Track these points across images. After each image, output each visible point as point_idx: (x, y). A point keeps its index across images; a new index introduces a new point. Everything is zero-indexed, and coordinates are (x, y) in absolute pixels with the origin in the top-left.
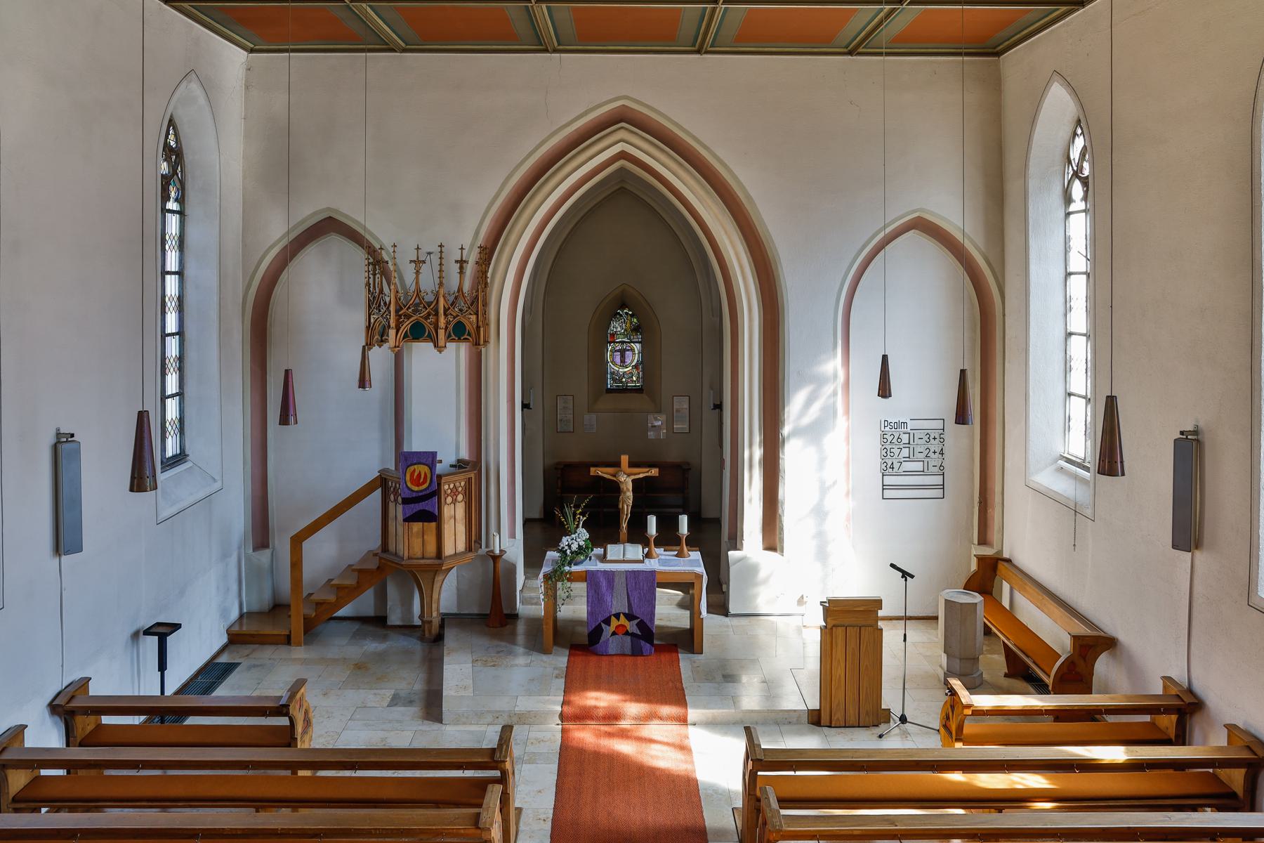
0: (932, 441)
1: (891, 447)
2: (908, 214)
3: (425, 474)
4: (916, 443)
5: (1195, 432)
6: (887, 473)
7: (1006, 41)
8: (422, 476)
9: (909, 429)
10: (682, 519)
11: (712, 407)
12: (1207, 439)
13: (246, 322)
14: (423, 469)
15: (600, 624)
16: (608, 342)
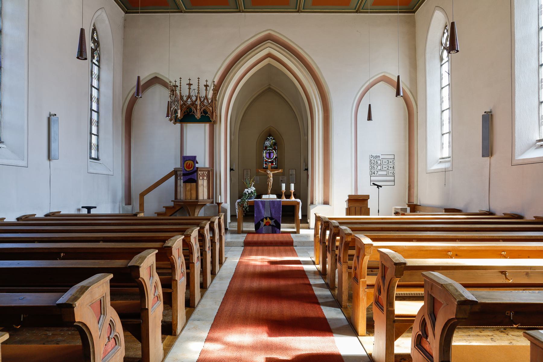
0: (390, 163)
1: (373, 165)
2: (379, 74)
3: (192, 164)
4: (383, 164)
5: (491, 112)
6: (372, 175)
7: (417, 4)
8: (191, 165)
9: (380, 158)
10: (292, 185)
11: (304, 169)
12: (493, 113)
13: (123, 116)
14: (190, 162)
15: (259, 221)
16: (264, 150)
